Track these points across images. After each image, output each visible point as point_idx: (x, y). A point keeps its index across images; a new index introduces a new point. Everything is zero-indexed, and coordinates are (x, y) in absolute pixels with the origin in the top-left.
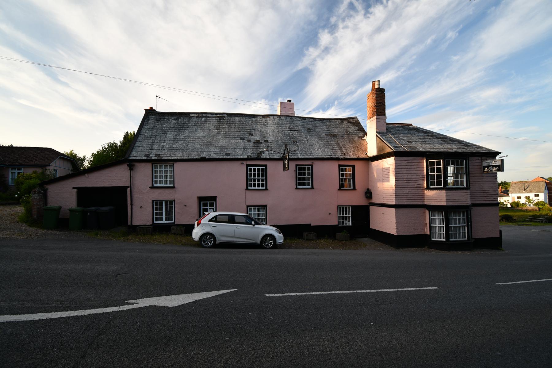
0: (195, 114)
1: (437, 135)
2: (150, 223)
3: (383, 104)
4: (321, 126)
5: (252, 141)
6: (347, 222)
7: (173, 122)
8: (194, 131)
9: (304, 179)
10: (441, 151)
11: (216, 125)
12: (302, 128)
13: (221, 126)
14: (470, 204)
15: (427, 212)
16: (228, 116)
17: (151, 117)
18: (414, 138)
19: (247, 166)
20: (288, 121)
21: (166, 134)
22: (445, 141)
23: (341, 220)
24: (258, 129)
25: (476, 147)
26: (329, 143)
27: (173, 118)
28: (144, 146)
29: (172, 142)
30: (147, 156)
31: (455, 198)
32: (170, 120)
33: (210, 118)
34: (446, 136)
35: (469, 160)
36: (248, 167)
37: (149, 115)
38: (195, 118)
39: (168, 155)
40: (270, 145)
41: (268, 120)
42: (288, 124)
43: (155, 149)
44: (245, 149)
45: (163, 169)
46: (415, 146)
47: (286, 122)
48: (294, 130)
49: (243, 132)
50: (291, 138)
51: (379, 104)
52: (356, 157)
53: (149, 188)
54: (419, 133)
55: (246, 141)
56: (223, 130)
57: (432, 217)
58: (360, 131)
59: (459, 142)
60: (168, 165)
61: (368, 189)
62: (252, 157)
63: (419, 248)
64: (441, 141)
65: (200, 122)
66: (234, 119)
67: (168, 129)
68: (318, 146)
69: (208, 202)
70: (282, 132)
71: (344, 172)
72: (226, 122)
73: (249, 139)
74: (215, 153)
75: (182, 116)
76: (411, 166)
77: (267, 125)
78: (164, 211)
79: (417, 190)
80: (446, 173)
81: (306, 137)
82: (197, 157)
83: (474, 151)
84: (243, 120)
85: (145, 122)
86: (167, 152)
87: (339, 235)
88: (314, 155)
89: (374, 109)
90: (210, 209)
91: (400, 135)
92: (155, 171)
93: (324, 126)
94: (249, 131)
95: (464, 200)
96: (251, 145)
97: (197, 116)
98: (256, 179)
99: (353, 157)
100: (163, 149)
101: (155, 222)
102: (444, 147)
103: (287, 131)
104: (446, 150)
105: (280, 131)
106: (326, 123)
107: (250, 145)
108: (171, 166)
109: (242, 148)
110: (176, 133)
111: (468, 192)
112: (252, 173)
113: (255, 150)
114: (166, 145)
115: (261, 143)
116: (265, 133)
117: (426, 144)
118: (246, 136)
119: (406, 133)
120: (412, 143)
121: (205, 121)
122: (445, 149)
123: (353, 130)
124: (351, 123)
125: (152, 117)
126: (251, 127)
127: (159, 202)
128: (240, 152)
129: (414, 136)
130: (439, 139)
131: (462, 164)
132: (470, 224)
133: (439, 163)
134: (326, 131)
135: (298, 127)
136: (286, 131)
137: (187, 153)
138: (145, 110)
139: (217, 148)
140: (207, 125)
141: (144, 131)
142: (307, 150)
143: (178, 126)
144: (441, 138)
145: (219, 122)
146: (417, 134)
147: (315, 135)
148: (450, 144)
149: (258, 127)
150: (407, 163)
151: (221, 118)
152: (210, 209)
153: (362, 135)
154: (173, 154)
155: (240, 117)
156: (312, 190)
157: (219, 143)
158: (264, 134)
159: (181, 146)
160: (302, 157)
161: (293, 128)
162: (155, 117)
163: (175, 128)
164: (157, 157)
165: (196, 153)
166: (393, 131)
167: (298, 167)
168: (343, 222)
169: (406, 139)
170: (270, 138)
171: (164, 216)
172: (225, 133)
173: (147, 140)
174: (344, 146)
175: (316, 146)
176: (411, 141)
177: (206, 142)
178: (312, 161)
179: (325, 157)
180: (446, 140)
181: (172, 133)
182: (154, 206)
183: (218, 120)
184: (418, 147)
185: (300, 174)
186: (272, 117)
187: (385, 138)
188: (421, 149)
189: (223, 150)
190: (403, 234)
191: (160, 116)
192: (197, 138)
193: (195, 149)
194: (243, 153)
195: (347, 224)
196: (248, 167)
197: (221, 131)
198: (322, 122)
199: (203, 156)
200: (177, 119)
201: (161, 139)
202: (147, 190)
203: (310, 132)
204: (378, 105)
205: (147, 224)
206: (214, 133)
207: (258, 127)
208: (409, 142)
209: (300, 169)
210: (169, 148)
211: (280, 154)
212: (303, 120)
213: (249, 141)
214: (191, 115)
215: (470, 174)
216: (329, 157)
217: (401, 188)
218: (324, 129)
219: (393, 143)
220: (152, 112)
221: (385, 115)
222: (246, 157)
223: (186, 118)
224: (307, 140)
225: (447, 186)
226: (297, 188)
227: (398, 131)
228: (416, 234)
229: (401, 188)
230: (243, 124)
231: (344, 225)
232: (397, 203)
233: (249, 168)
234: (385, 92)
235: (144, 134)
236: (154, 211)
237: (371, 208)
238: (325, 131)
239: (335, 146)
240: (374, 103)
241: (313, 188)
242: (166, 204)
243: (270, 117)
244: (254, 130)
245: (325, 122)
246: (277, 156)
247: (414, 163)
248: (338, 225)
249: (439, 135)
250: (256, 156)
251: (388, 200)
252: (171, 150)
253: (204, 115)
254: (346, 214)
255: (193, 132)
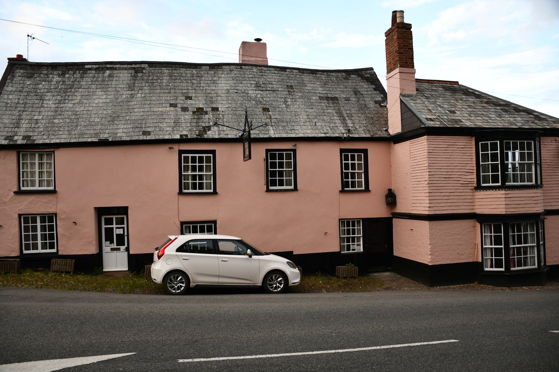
0: (94, 64)
1: (495, 100)
2: (16, 253)
3: (409, 49)
4: (313, 82)
5: (190, 109)
6: (356, 247)
7: (55, 80)
8: (91, 93)
9: (281, 174)
10: (498, 127)
11: (129, 82)
12: (278, 86)
13: (136, 85)
14: (543, 211)
15: (478, 225)
16: (150, 67)
17: (17, 71)
18: (459, 104)
19: (181, 152)
20: (255, 73)
21: (43, 100)
22: (506, 111)
23: (346, 244)
24: (201, 88)
25: (552, 120)
26: (325, 111)
27: (55, 73)
28: (5, 122)
29: (53, 113)
30: (10, 138)
31: (518, 202)
32: (51, 76)
33: (119, 71)
34: (509, 102)
35: (541, 141)
36: (183, 155)
37: (14, 68)
38: (94, 72)
39: (45, 137)
40: (221, 116)
41: (220, 72)
42: (254, 79)
43: (23, 126)
44: (177, 123)
45: (37, 161)
46: (459, 118)
47: (251, 76)
48: (264, 89)
49: (175, 93)
50: (258, 102)
51: (403, 48)
52: (368, 136)
53: (14, 194)
54: (467, 97)
55: (180, 110)
56: (140, 92)
57: (484, 233)
58: (378, 92)
59: (527, 112)
60: (29, 153)
61: (390, 190)
62: (189, 137)
63: (465, 285)
64: (501, 111)
65: (101, 78)
66: (160, 71)
67: (46, 91)
68: (305, 117)
69: (114, 217)
70: (243, 93)
71: (350, 162)
72: (146, 78)
73: (185, 106)
74: (125, 131)
75: (71, 69)
76: (453, 152)
77: (218, 82)
78: (39, 233)
79: (462, 191)
80: (506, 162)
81: (285, 102)
82: (93, 139)
83: (548, 127)
84: (176, 72)
85: (7, 80)
86: (44, 131)
87: (341, 269)
88: (297, 132)
89: (396, 57)
90: (117, 228)
91: (438, 100)
92: (23, 164)
93: (318, 83)
94: (186, 91)
95: (533, 205)
96: (188, 116)
97: (97, 68)
98: (196, 175)
99: (365, 136)
100: (37, 126)
101: (25, 252)
102: (503, 120)
103: (252, 93)
104: (507, 125)
105: (239, 91)
106: (320, 78)
107: (186, 117)
108: (50, 154)
109: (173, 121)
110: (59, 98)
111: (537, 193)
112: (190, 164)
113: (195, 124)
114: (42, 119)
115: (206, 113)
116: (213, 95)
117: (477, 115)
118: (181, 101)
119: (449, 96)
120: (456, 113)
121: (110, 76)
122: (504, 124)
123: (366, 90)
124: (363, 78)
125: (19, 72)
126: (189, 84)
127: (31, 217)
128: (168, 129)
129: (461, 101)
130: (498, 108)
131: (529, 148)
132: (541, 243)
133: (494, 147)
134: (320, 92)
135: (271, 84)
136: (250, 92)
137: (76, 132)
138: (9, 59)
139: (129, 122)
140: (114, 83)
141: (6, 96)
142: (285, 124)
143: (63, 86)
144: (500, 105)
145: (135, 77)
146: (464, 99)
147: (302, 97)
148: (513, 116)
149: (202, 85)
150: (447, 146)
151: (137, 71)
152: (117, 228)
153: (380, 99)
154: (54, 135)
155: (172, 69)
156: (294, 194)
157: (132, 114)
158: (212, 98)
159: (68, 120)
160: (277, 136)
161: (263, 86)
162: (25, 71)
163: (58, 90)
164: (25, 141)
165: (92, 132)
166: (427, 94)
167: (271, 154)
168: (348, 247)
169: (446, 106)
170: (222, 104)
171: (39, 242)
172: (143, 95)
173: (10, 112)
174: (350, 116)
175: (301, 117)
176: (453, 109)
177: (110, 112)
178: (294, 144)
179: (316, 136)
180: (509, 108)
181: (54, 98)
182: (23, 225)
183: (133, 74)
184: (463, 121)
185: (273, 165)
186: (227, 67)
187: (414, 105)
188: (468, 124)
189: (140, 126)
190: (440, 263)
191: (34, 70)
192: (94, 105)
193: (91, 124)
194: (173, 131)
195: (355, 250)
196: (183, 155)
197: (136, 92)
198: (314, 75)
199: (103, 136)
200: (62, 74)
201: (34, 109)
202: (10, 197)
203: (293, 93)
204: (402, 51)
205: (11, 256)
206: (125, 97)
207: (202, 85)
208: (452, 112)
209: (273, 157)
210: (47, 124)
211: (237, 132)
212: (282, 72)
213: (185, 109)
214: (86, 67)
215: (542, 164)
216: (323, 135)
217: (438, 188)
218: (316, 88)
219: (424, 113)
220: (20, 62)
221: (413, 66)
222: (178, 137)
223: (77, 72)
224: (287, 106)
225: (507, 184)
226: (268, 190)
227: (436, 93)
228: (461, 262)
229: (438, 188)
230: (176, 79)
231: (351, 251)
232: (432, 213)
233: (184, 157)
234: (412, 30)
235: (5, 101)
236: (23, 234)
237: (395, 221)
238: (318, 92)
239: (335, 117)
240: (396, 47)
241: (296, 189)
242: (43, 220)
243: (224, 67)
244: (194, 91)
245: (320, 76)
246: (233, 134)
247: (458, 146)
248: (340, 252)
249: (499, 101)
250: (197, 135)
251: (418, 208)
252: (51, 128)
253: (108, 66)
254: (354, 233)
255: (88, 96)
